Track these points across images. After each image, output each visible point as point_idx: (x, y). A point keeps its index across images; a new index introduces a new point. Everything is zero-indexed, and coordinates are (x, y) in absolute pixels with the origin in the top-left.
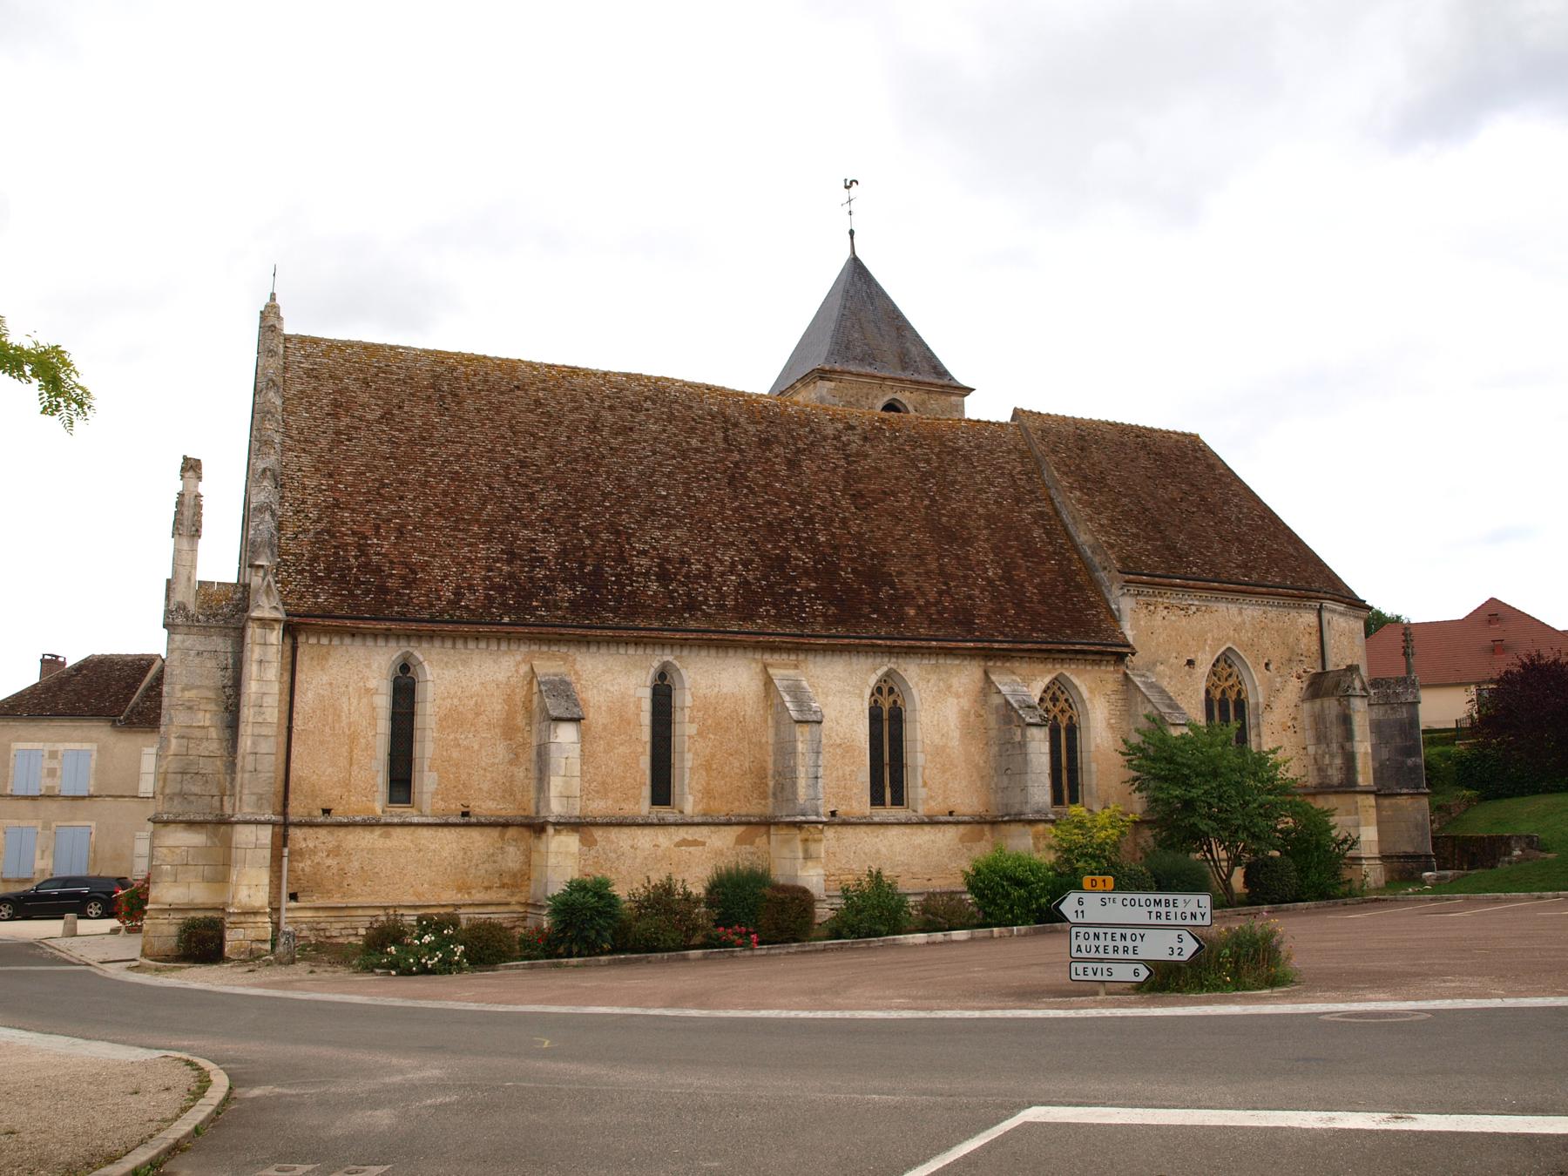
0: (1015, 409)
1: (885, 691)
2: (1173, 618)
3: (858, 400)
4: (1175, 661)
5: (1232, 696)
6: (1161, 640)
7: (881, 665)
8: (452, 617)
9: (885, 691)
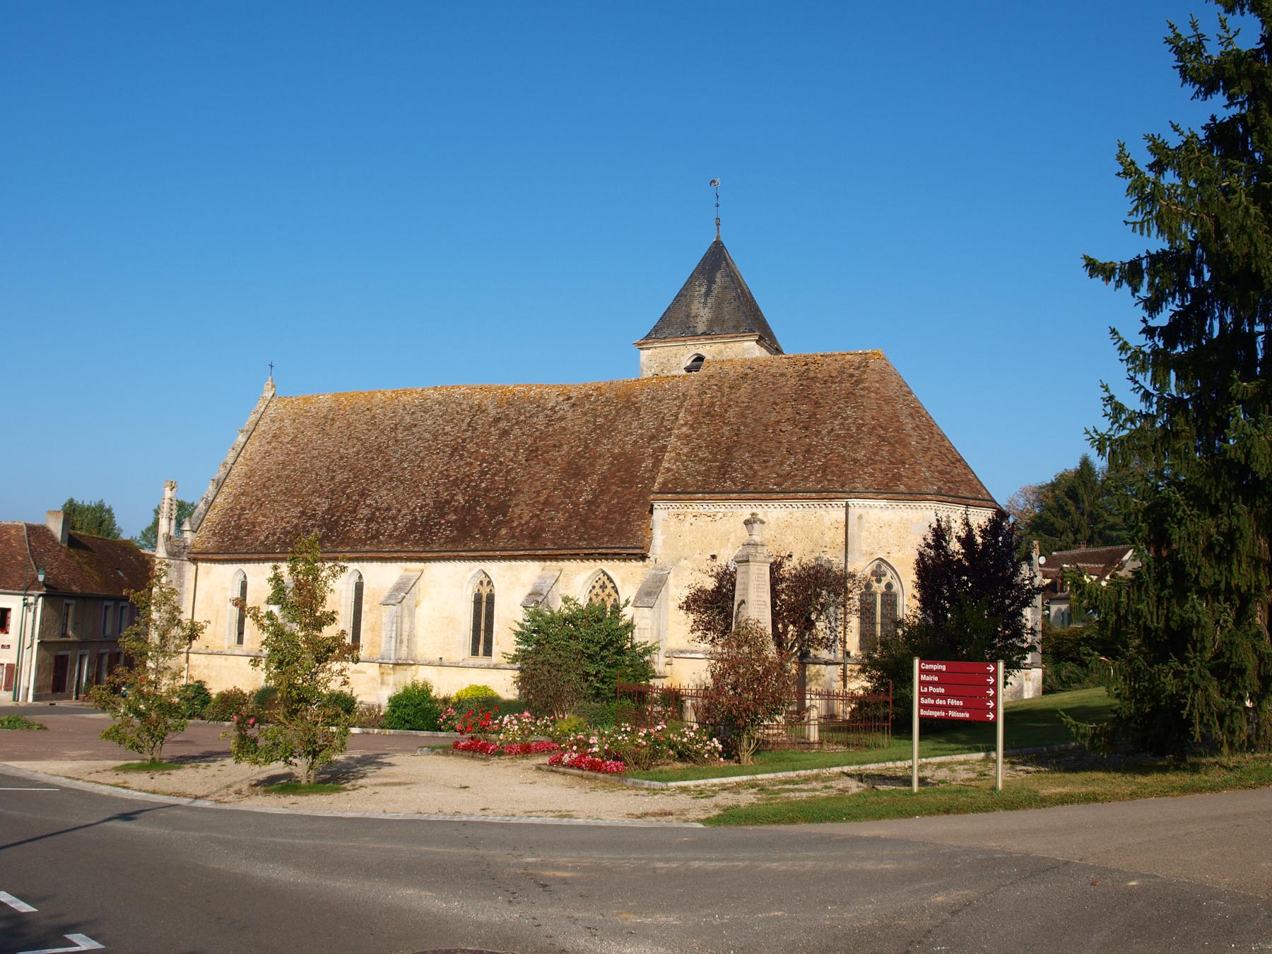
0: (71, 501)
1: (485, 583)
2: (700, 523)
3: (668, 360)
4: (698, 556)
6: (688, 541)
7: (475, 567)
8: (909, 487)
9: (485, 583)
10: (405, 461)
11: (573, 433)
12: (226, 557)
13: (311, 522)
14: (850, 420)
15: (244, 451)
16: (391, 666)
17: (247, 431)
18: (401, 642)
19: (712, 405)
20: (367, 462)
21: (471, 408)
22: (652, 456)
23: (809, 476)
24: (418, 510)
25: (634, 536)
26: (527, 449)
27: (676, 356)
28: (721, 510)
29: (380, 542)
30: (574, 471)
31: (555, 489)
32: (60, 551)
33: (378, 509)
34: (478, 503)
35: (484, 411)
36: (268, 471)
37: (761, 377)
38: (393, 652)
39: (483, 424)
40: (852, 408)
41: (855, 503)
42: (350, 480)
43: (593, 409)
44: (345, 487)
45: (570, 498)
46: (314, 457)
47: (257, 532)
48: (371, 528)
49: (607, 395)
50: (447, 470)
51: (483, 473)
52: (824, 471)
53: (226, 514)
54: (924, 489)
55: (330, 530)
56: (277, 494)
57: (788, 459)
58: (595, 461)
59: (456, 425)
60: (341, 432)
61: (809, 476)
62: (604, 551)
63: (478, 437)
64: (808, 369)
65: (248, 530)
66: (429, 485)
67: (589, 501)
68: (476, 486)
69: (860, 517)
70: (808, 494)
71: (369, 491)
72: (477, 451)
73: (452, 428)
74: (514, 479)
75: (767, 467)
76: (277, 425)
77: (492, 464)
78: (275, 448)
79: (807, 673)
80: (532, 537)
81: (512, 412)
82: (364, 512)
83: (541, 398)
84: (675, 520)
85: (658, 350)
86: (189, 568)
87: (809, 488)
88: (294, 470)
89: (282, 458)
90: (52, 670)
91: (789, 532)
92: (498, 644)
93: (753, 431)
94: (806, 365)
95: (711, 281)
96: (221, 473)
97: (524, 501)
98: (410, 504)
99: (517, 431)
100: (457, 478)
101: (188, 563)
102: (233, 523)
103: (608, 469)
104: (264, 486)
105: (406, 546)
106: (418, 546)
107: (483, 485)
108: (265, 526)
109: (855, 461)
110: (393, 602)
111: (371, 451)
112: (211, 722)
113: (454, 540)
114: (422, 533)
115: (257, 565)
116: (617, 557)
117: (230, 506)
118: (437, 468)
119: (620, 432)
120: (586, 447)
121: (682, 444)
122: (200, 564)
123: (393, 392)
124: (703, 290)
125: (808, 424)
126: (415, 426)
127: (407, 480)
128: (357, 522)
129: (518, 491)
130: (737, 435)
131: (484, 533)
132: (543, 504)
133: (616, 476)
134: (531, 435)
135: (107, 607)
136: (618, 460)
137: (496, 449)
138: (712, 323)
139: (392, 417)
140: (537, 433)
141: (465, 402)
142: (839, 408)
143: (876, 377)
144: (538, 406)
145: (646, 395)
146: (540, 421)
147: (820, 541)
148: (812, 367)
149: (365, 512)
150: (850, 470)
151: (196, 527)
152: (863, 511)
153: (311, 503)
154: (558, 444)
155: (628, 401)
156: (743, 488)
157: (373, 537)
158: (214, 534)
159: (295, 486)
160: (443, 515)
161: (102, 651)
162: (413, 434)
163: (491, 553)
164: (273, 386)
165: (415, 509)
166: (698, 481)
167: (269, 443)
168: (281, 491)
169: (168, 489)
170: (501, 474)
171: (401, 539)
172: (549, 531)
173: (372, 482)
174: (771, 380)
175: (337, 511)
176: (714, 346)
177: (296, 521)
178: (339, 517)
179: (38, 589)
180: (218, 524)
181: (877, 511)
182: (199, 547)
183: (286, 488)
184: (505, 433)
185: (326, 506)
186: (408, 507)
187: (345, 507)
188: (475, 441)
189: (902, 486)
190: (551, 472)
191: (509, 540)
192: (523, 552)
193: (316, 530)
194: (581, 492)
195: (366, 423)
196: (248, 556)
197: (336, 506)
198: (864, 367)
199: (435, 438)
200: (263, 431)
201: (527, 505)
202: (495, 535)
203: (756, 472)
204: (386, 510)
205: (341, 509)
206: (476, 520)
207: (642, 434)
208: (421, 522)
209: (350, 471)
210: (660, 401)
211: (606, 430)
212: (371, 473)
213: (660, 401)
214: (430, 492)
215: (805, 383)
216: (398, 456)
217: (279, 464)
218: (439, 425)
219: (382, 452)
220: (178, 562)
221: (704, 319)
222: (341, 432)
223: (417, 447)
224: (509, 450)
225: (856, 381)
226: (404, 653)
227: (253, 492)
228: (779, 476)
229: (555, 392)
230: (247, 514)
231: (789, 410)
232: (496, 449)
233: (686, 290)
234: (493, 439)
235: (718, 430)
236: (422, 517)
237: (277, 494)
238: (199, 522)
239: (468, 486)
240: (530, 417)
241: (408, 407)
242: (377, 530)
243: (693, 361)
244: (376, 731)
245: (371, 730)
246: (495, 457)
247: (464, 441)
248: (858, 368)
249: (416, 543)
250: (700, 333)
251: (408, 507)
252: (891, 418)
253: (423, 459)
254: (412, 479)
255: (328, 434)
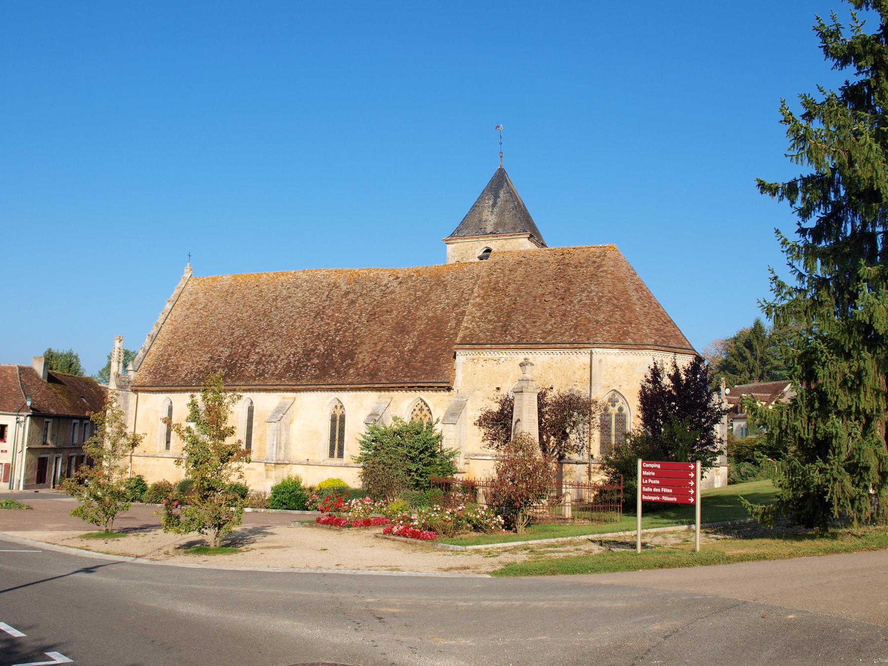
1: (339, 407)
2: (489, 365)
3: (467, 251)
5: (613, 411)
6: (480, 378)
8: (634, 340)
9: (339, 407)
10: (283, 322)
11: (400, 302)
12: (157, 389)
13: (217, 364)
14: (593, 294)
15: (170, 315)
16: (273, 465)
17: (173, 301)
18: (280, 448)
19: (497, 282)
20: (256, 323)
21: (329, 285)
22: (455, 318)
23: (565, 332)
24: (292, 356)
25: (443, 374)
26: (368, 313)
27: (477, 247)
28: (503, 356)
29: (265, 378)
30: (401, 329)
31: (388, 341)
32: (42, 385)
33: (264, 355)
34: (334, 351)
35: (338, 287)
36: (187, 329)
37: (531, 263)
38: (274, 455)
39: (337, 296)
40: (595, 285)
41: (597, 351)
42: (245, 335)
43: (414, 286)
44: (241, 340)
45: (398, 348)
46: (219, 319)
47: (179, 371)
48: (259, 369)
49: (424, 276)
50: (312, 328)
51: (337, 330)
52: (575, 329)
53: (158, 359)
54: (645, 341)
55: (231, 370)
56: (194, 345)
57: (550, 320)
58: (415, 322)
59: (319, 297)
60: (238, 302)
61: (565, 332)
62: (422, 385)
63: (334, 305)
64: (564, 258)
65: (173, 370)
66: (299, 339)
67: (411, 350)
68: (333, 339)
69: (600, 361)
70: (564, 345)
71: (258, 343)
72: (333, 315)
73: (316, 299)
74: (359, 334)
75: (535, 326)
76: (194, 297)
77: (344, 324)
78: (192, 313)
79: (563, 470)
80: (372, 375)
81: (357, 288)
82: (254, 357)
83: (377, 278)
84: (471, 363)
85: (459, 245)
86: (132, 396)
87: (565, 340)
88: (205, 328)
89: (197, 320)
90: (37, 468)
91: (551, 371)
92: (347, 450)
93: (526, 301)
94: (563, 254)
95: (496, 196)
96: (154, 331)
97: (366, 350)
98: (286, 352)
99: (361, 301)
100: (319, 334)
101: (132, 393)
102: (163, 365)
103: (424, 327)
104: (185, 339)
105: (284, 381)
106: (292, 381)
107: (337, 339)
108: (185, 367)
109: (597, 322)
110: (275, 420)
111: (259, 315)
112: (148, 504)
113: (317, 377)
114: (294, 372)
115: (179, 394)
116: (431, 389)
117: (161, 353)
118: (305, 327)
119: (432, 302)
120: (409, 312)
121: (476, 310)
122: (139, 394)
123: (275, 274)
124: (491, 203)
125: (564, 297)
126: (290, 297)
127: (284, 335)
128: (249, 365)
129: (362, 343)
130: (514, 303)
131: (338, 372)
132: (379, 352)
133: (430, 333)
134: (371, 304)
135: (75, 424)
136: (432, 321)
137: (346, 313)
138: (497, 225)
139: (273, 291)
140: (375, 303)
141: (325, 281)
142: (585, 285)
143: (612, 263)
144: (376, 284)
145: (451, 275)
146: (377, 294)
147: (573, 377)
148: (567, 256)
149: (255, 357)
150: (593, 328)
151: (137, 368)
152: (602, 357)
153: (217, 351)
154: (389, 310)
155: (438, 280)
156: (519, 341)
157: (260, 375)
158: (150, 373)
159: (206, 339)
160: (309, 360)
161: (71, 454)
162: (288, 303)
163: (343, 386)
164: (191, 270)
165: (290, 355)
166: (487, 336)
167: (188, 309)
168: (196, 343)
169: (117, 341)
170: (350, 331)
171: (280, 377)
172: (383, 371)
173: (260, 337)
174: (538, 265)
175: (236, 357)
176: (499, 242)
177: (206, 364)
178: (237, 361)
179: (27, 411)
180: (152, 366)
181: (612, 356)
182: (139, 382)
183: (200, 341)
184: (353, 302)
185: (227, 353)
186: (285, 354)
187: (241, 354)
188: (332, 308)
189: (630, 340)
190: (384, 329)
191: (355, 377)
192: (365, 386)
193: (221, 370)
194: (406, 343)
195: (255, 296)
196: (173, 388)
197: (235, 354)
198: (603, 256)
199: (304, 306)
200: (184, 301)
201: (368, 353)
202: (345, 374)
203: (527, 330)
204: (270, 356)
205: (238, 356)
206: (333, 363)
207: (448, 303)
208: (294, 364)
209: (244, 329)
210: (460, 280)
211: (423, 300)
212: (259, 330)
213: (460, 280)
214: (300, 343)
215: (562, 267)
216: (278, 318)
217: (195, 324)
218: (306, 297)
219: (267, 315)
220: (125, 392)
221: (492, 223)
222: (238, 302)
223: (291, 312)
224: (355, 314)
225: (597, 266)
226: (282, 456)
227: (176, 344)
228: (544, 332)
229: (387, 273)
230: (173, 359)
231: (551, 286)
232: (346, 313)
233: (479, 202)
234: (344, 307)
235: (501, 300)
236: (295, 361)
237: (194, 345)
238: (139, 364)
239: (327, 339)
240: (370, 291)
241: (285, 284)
242: (263, 370)
243: (484, 252)
244: (263, 510)
245: (259, 510)
246: (346, 319)
247: (324, 308)
248: (599, 257)
249: (291, 379)
250: (488, 232)
251: (285, 354)
252: (622, 292)
253: (295, 321)
254: (288, 335)
255: (229, 303)
